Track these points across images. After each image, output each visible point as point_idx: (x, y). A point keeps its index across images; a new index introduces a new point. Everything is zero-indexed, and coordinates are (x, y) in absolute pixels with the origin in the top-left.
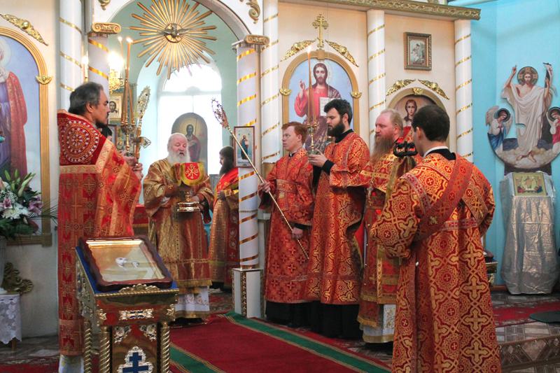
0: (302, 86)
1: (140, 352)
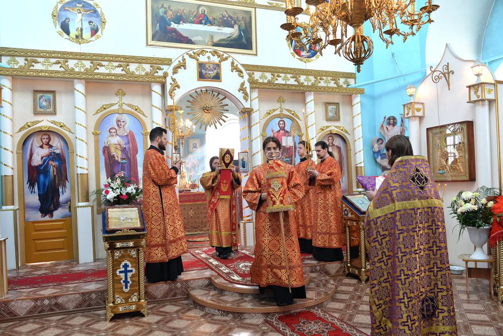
1: (128, 263)
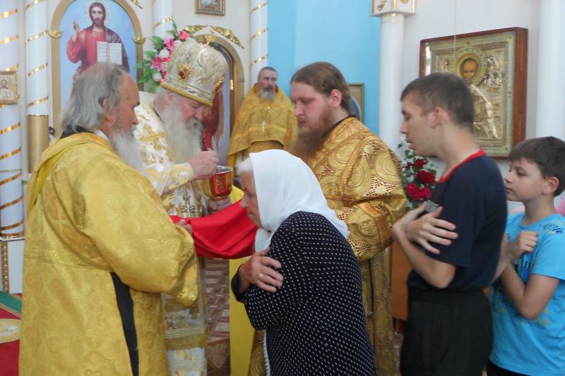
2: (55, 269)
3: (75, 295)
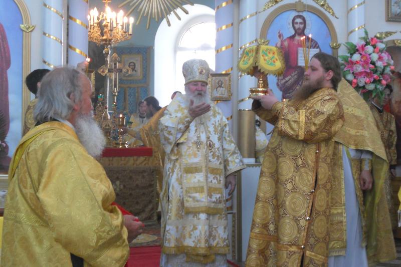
0: (280, 36)
2: (23, 228)
3: (37, 249)
